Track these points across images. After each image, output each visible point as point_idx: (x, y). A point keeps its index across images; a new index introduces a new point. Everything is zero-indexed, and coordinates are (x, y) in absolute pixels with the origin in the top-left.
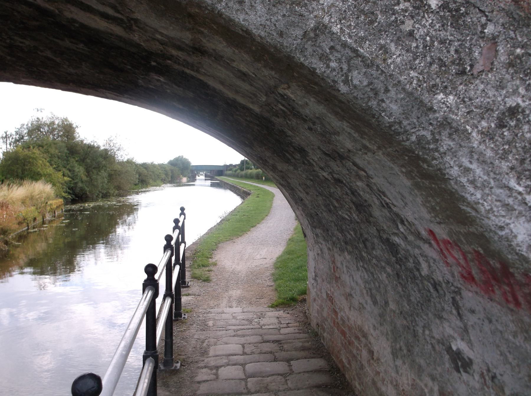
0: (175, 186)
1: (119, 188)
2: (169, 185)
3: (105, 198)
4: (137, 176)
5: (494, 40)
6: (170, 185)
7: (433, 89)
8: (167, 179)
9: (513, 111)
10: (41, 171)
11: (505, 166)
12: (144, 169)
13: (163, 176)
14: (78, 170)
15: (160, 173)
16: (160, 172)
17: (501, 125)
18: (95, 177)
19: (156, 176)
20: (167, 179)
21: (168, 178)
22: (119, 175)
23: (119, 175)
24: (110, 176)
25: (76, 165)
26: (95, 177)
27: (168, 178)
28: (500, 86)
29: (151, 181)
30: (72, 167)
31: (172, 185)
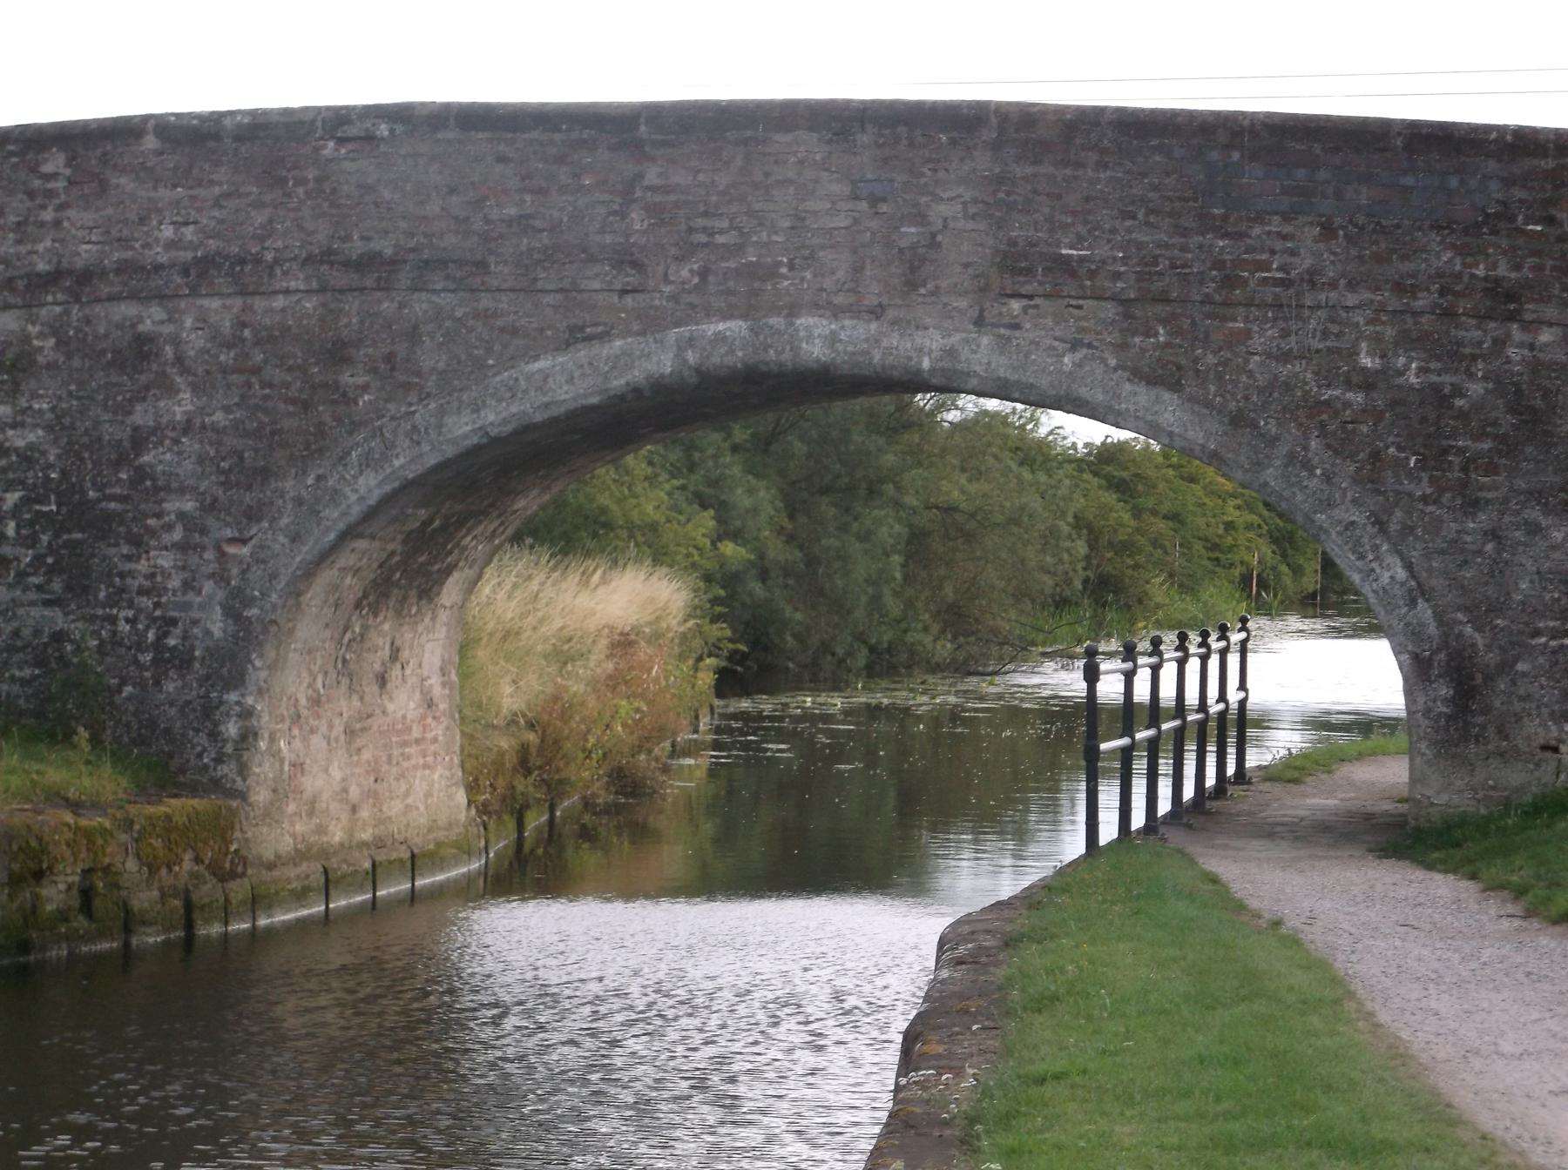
0: (1338, 633)
1: (956, 619)
2: (1294, 622)
3: (880, 676)
4: (1081, 548)
5: (1345, 489)
6: (1307, 624)
7: (1315, 512)
8: (1287, 580)
9: (1353, 523)
10: (614, 507)
11: (1346, 548)
12: (1110, 498)
13: (1258, 553)
14: (747, 503)
15: (1229, 526)
16: (1232, 514)
17: (1347, 529)
18: (833, 542)
19: (1198, 546)
20: (1287, 580)
21: (1297, 571)
22: (969, 537)
23: (969, 537)
24: (916, 545)
25: (736, 471)
26: (833, 542)
27: (1297, 571)
28: (1346, 512)
29: (1158, 588)
30: (714, 483)
31: (1319, 625)
